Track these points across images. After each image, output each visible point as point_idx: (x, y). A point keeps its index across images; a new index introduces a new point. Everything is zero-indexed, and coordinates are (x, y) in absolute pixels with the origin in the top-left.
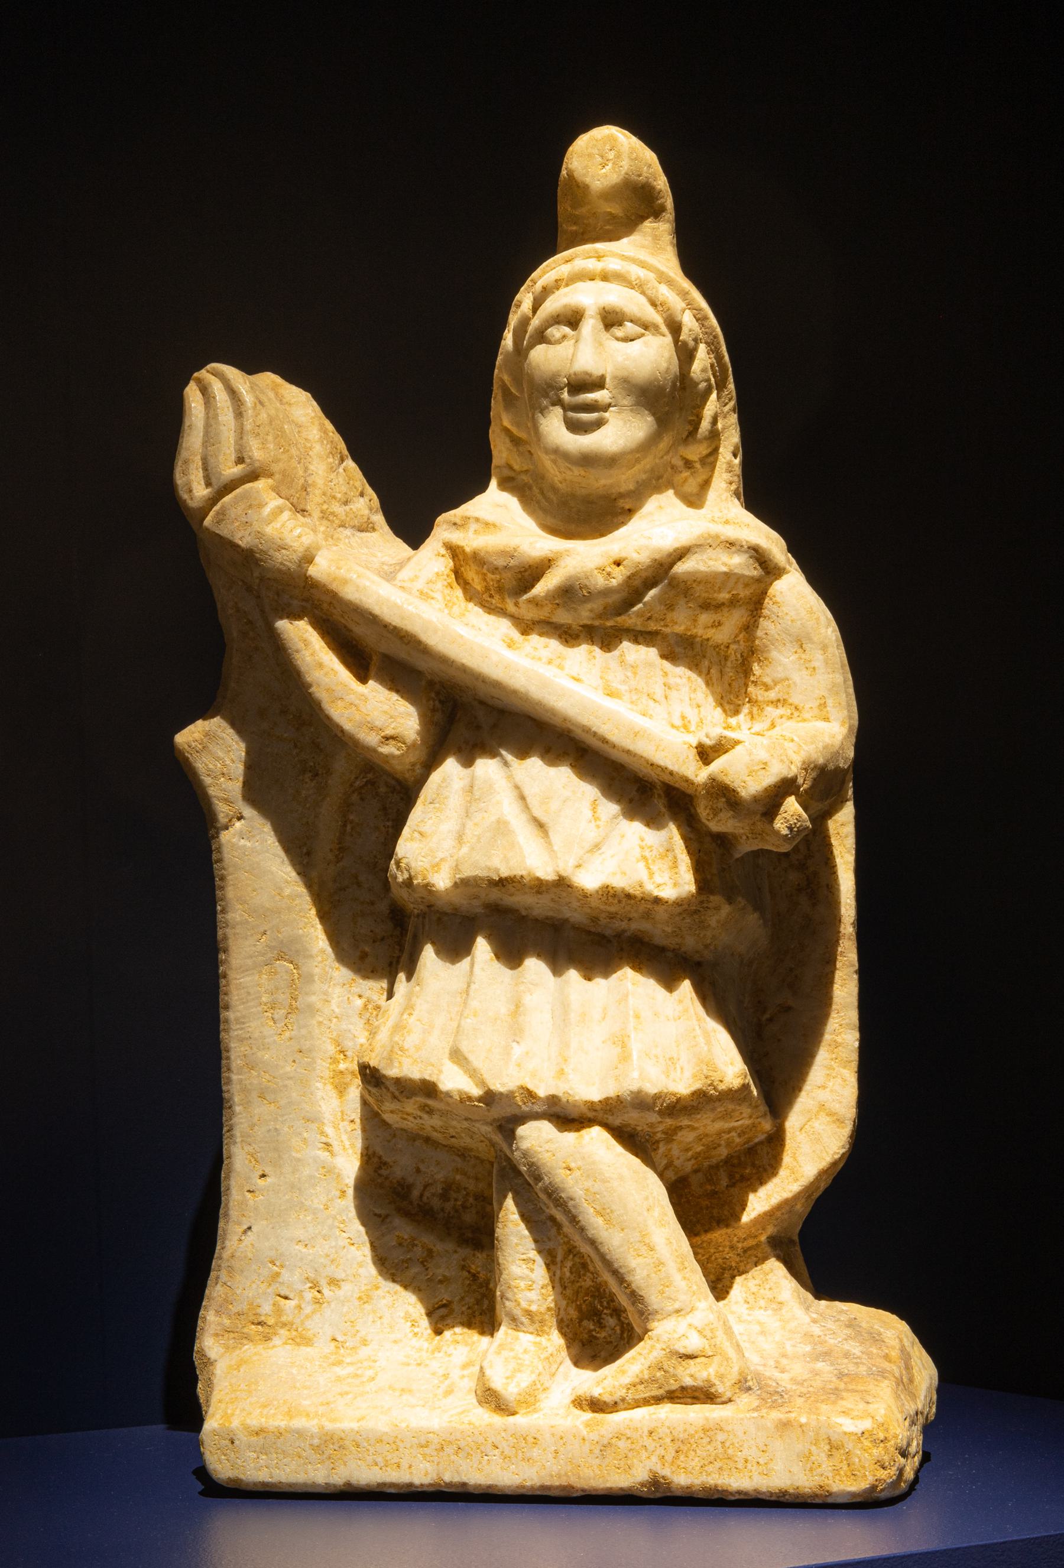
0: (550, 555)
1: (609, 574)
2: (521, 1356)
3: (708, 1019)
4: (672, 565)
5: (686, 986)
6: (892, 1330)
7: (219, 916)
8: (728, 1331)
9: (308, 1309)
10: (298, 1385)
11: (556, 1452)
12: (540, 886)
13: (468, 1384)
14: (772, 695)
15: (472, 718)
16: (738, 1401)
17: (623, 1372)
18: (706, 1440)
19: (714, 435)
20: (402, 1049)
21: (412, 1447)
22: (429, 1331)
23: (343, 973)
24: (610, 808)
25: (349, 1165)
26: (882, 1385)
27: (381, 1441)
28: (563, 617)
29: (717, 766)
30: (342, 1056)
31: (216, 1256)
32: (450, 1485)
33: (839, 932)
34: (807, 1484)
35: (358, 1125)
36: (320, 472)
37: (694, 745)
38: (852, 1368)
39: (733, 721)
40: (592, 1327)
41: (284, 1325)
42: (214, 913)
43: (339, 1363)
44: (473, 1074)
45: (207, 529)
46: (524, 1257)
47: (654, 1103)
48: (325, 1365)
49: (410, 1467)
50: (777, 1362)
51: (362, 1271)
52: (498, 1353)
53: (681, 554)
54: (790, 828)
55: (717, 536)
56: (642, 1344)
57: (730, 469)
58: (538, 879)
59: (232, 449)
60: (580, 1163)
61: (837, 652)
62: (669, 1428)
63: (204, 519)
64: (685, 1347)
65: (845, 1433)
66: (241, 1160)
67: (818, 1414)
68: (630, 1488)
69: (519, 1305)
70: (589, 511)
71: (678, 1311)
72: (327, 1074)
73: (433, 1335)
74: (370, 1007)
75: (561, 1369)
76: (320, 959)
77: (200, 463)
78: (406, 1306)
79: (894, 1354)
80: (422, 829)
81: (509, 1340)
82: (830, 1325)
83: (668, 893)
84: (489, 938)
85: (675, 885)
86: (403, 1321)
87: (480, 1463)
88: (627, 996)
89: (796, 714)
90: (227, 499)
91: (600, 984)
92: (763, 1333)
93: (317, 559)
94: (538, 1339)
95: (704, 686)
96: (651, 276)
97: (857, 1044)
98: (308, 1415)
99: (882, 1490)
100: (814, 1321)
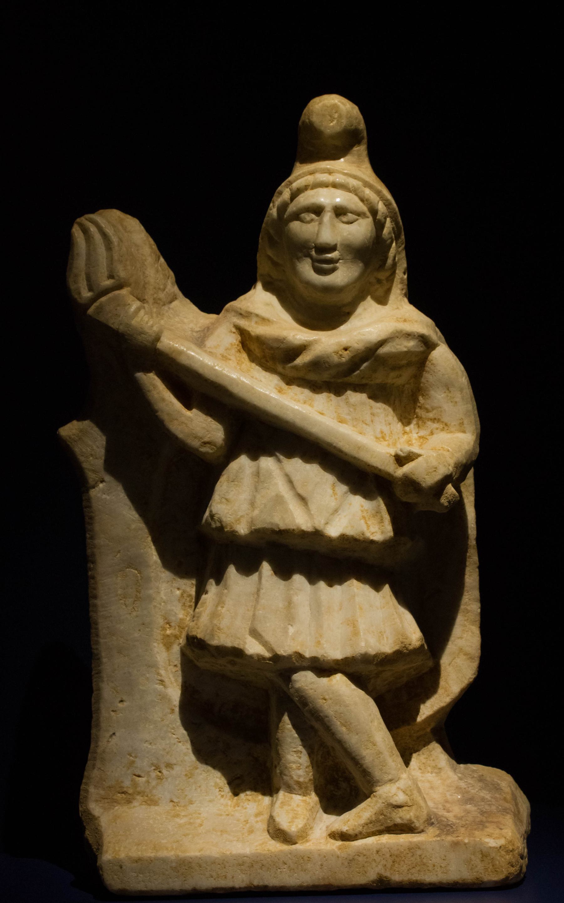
0: (306, 343)
1: (341, 355)
2: (296, 809)
3: (399, 606)
4: (377, 349)
5: (387, 589)
6: (504, 780)
7: (88, 541)
8: (419, 791)
9: (154, 783)
10: (156, 830)
11: (322, 865)
12: (303, 534)
13: (261, 825)
14: (431, 415)
15: (259, 433)
16: (427, 831)
17: (360, 817)
18: (410, 855)
19: (394, 265)
20: (219, 629)
21: (233, 865)
22: (230, 794)
23: (166, 575)
24: (343, 488)
25: (175, 693)
26: (506, 817)
27: (215, 863)
28: (312, 377)
29: (407, 468)
30: (168, 626)
31: (91, 751)
32: (258, 887)
33: (468, 544)
34: (469, 877)
35: (179, 668)
36: (152, 275)
37: (393, 454)
38: (487, 807)
39: (407, 429)
40: (332, 789)
41: (139, 793)
42: (85, 538)
43: (178, 816)
44: (265, 644)
45: (90, 316)
46: (295, 750)
47: (374, 660)
48: (169, 817)
49: (233, 877)
50: (444, 806)
51: (186, 758)
52: (282, 807)
53: (382, 343)
54: (449, 502)
55: (401, 331)
56: (369, 799)
57: (402, 282)
58: (303, 531)
59: (105, 269)
60: (331, 696)
61: (468, 391)
62: (388, 848)
63: (88, 309)
64: (396, 801)
65: (491, 847)
66: (107, 690)
67: (475, 837)
68: (365, 885)
69: (292, 778)
70: (325, 312)
71: (391, 780)
72: (160, 637)
73: (233, 796)
74: (185, 595)
75: (318, 815)
76: (154, 567)
77: (84, 277)
78: (214, 780)
79: (509, 797)
80: (228, 497)
81: (287, 799)
82: (470, 781)
83: (378, 537)
84: (271, 563)
85: (382, 533)
86: (214, 788)
87: (276, 873)
88: (354, 596)
89: (446, 428)
90: (103, 299)
91: (337, 589)
92: (432, 788)
93: (162, 339)
94: (304, 798)
95: (392, 412)
96: (360, 183)
97: (479, 610)
98: (167, 849)
99: (512, 879)
100: (461, 779)
